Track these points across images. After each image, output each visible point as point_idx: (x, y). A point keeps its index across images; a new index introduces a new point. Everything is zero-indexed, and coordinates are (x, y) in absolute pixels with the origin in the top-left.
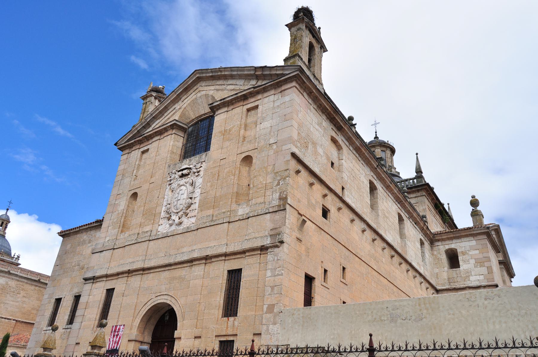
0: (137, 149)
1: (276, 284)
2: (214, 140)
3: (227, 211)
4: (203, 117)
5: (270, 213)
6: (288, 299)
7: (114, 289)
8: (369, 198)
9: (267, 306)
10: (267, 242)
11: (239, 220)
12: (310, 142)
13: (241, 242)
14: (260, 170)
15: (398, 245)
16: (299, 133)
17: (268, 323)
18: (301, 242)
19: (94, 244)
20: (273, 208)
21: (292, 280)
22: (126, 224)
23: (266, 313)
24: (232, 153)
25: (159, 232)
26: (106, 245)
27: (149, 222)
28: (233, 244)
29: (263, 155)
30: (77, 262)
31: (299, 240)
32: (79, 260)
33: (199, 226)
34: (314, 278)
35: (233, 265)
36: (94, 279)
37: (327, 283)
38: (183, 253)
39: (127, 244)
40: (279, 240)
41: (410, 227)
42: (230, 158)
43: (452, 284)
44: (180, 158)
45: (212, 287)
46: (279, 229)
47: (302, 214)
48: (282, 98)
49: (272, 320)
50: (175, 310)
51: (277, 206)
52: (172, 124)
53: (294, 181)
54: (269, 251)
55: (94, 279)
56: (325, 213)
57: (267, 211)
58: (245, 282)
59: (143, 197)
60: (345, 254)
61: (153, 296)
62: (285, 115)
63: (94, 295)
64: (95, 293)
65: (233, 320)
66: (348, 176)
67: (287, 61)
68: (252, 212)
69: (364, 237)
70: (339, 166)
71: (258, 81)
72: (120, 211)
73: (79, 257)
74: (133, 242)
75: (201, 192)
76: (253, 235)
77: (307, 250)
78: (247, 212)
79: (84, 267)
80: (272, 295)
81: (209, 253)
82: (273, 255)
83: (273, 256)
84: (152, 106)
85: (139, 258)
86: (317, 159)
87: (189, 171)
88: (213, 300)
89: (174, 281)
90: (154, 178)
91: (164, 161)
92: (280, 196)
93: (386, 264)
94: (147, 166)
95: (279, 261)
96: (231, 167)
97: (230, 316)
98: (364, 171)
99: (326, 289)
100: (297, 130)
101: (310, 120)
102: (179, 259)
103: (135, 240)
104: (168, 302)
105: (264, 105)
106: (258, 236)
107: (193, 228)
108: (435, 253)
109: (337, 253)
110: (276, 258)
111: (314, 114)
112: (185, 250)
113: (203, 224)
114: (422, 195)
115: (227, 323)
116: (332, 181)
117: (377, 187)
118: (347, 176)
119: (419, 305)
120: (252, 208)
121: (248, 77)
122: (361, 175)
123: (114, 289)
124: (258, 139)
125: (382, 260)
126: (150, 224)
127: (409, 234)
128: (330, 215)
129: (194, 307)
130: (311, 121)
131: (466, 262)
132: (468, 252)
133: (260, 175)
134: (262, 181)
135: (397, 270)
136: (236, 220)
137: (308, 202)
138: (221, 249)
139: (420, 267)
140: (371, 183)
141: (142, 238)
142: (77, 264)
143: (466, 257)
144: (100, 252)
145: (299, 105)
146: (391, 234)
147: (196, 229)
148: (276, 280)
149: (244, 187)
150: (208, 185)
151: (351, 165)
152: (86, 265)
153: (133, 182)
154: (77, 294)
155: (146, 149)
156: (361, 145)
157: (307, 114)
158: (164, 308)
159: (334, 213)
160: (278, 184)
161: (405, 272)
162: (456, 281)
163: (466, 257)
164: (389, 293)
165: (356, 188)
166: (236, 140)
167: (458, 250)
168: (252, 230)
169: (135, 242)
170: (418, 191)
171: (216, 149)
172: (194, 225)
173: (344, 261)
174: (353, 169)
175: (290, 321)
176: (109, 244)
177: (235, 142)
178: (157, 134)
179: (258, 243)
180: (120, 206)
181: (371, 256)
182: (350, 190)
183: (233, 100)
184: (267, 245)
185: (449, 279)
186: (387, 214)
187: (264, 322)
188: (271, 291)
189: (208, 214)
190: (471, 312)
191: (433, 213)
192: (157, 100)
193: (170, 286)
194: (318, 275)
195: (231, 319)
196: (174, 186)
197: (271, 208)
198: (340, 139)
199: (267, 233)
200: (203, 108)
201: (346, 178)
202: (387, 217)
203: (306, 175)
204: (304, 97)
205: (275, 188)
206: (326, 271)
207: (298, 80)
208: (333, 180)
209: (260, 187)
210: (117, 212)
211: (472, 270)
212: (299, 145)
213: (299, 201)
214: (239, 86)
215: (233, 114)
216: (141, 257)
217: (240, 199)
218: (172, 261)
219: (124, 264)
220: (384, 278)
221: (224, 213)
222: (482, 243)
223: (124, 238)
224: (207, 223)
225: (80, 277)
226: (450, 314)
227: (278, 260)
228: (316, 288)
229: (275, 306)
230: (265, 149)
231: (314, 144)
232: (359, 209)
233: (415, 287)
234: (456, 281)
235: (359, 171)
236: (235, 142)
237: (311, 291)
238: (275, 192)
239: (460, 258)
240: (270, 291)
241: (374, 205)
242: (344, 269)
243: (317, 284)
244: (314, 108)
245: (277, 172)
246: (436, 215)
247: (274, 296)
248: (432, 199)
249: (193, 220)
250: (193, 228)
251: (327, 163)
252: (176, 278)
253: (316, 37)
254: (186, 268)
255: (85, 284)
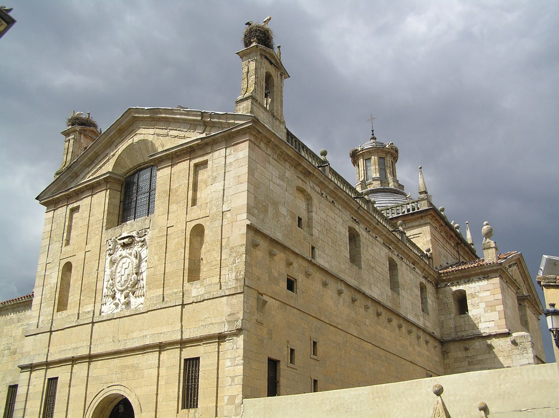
0: (64, 206)
1: (236, 375)
2: (158, 201)
3: (179, 292)
4: (142, 166)
5: (226, 296)
6: (249, 389)
7: (57, 378)
8: (348, 250)
9: (228, 397)
10: (225, 329)
11: (193, 302)
12: (270, 203)
13: (197, 329)
14: (213, 244)
15: (387, 298)
16: (255, 197)
17: (229, 415)
18: (262, 325)
19: (25, 323)
20: (229, 290)
21: (254, 368)
22: (62, 301)
23: (227, 404)
24: (180, 220)
25: (103, 312)
26: (41, 326)
27: (90, 301)
28: (188, 330)
29: (216, 225)
30: (6, 345)
31: (260, 323)
32: (8, 343)
33: (148, 308)
34: (279, 361)
35: (189, 352)
36: (31, 368)
37: (294, 364)
38: (133, 339)
39: (66, 327)
40: (237, 328)
41: (406, 271)
42: (178, 226)
43: (459, 333)
44: (118, 218)
45: (169, 377)
46: (236, 314)
47: (263, 293)
48: (235, 153)
49: (234, 411)
50: (131, 402)
51: (233, 289)
52: (105, 177)
53: (251, 256)
54: (228, 339)
55: (31, 368)
56: (291, 285)
57: (223, 294)
58: (204, 372)
59: (79, 269)
60: (316, 327)
61: (105, 387)
62: (239, 176)
63: (35, 386)
64: (35, 383)
65: (194, 412)
66: (319, 231)
67: (239, 104)
68: (207, 294)
69: (341, 300)
70: (308, 220)
71: (206, 128)
72: (52, 285)
73: (8, 339)
74: (74, 324)
75: (148, 266)
76: (210, 321)
77: (270, 333)
78: (202, 293)
79: (16, 352)
80: (233, 386)
81: (163, 339)
82: (231, 343)
83: (232, 345)
84: (77, 144)
85: (84, 343)
86: (279, 222)
87: (131, 240)
88: (171, 391)
89: (126, 370)
90: (90, 244)
91: (99, 224)
92: (236, 276)
93: (370, 326)
94: (80, 229)
95: (238, 349)
96: (180, 238)
97: (191, 408)
98: (341, 218)
99: (293, 370)
100: (254, 194)
101: (269, 175)
102: (130, 346)
103: (75, 322)
104: (122, 393)
105: (214, 160)
106: (215, 322)
107: (142, 310)
108: (441, 296)
109: (306, 327)
110: (235, 347)
111: (274, 166)
112: (135, 335)
113: (153, 305)
114: (426, 222)
115: (188, 415)
116: (299, 244)
117: (360, 233)
118: (318, 232)
119: (373, 394)
120: (206, 289)
121: (192, 125)
122: (337, 224)
123: (57, 378)
124: (209, 204)
125: (365, 321)
126: (91, 302)
127: (405, 280)
128: (296, 284)
129: (152, 399)
130: (271, 176)
131: (476, 306)
132: (477, 294)
133: (214, 250)
134: (216, 256)
135: (386, 330)
136: (190, 302)
137: (269, 277)
138: (175, 336)
139: (419, 319)
140: (351, 229)
141: (84, 320)
142: (6, 347)
143: (475, 301)
144: (35, 335)
145: (255, 161)
146: (378, 287)
147: (145, 311)
148: (236, 370)
149: (196, 261)
150: (155, 258)
151: (324, 216)
152: (18, 349)
153: (65, 248)
154: (12, 384)
155: (76, 205)
156: (336, 188)
157: (265, 168)
158: (117, 398)
159: (302, 281)
160: (234, 262)
161: (397, 329)
162: (464, 330)
163: (476, 300)
164: (373, 359)
165: (330, 243)
166: (184, 204)
167: (466, 291)
168: (208, 315)
169: (76, 324)
170: (422, 217)
171: (161, 213)
172: (143, 306)
173: (315, 334)
174: (326, 220)
175: (252, 412)
176: (45, 325)
177: (182, 206)
178: (88, 188)
179: (216, 330)
180: (52, 278)
181: (350, 320)
182: (322, 247)
183: (178, 152)
184: (225, 332)
185: (455, 327)
186: (373, 264)
187: (226, 414)
188: (231, 382)
189: (158, 294)
190: (416, 399)
191: (441, 243)
192: (82, 135)
193: (122, 375)
194: (283, 357)
195: (192, 411)
196: (117, 255)
197: (227, 290)
198: (309, 186)
199: (224, 319)
200: (141, 156)
201: (317, 235)
202: (373, 268)
203: (266, 245)
204: (261, 149)
205: (230, 266)
206: (292, 351)
207: (252, 131)
208: (299, 241)
209: (214, 264)
210: (49, 286)
211: (482, 316)
212: (256, 212)
213: (259, 279)
214: (183, 132)
215: (178, 169)
216: (85, 343)
217: (193, 276)
218: (121, 347)
219: (66, 350)
220: (368, 343)
221: (176, 293)
222: (493, 283)
223: (62, 318)
224: (158, 305)
225: (13, 363)
226: (398, 402)
227: (237, 348)
228: (281, 372)
229: (237, 398)
230: (217, 217)
231: (275, 204)
232: (334, 268)
233: (410, 345)
234: (464, 330)
235: (334, 220)
236: (182, 206)
237: (276, 376)
238: (231, 272)
239: (469, 302)
240: (230, 382)
241: (356, 256)
242: (315, 343)
243: (283, 367)
244: (274, 159)
245: (233, 248)
246: (445, 245)
247: (234, 387)
248: (440, 225)
249: (142, 300)
250: (142, 310)
251: (292, 223)
252: (129, 367)
253: (274, 64)
254: (138, 356)
255: (21, 372)
